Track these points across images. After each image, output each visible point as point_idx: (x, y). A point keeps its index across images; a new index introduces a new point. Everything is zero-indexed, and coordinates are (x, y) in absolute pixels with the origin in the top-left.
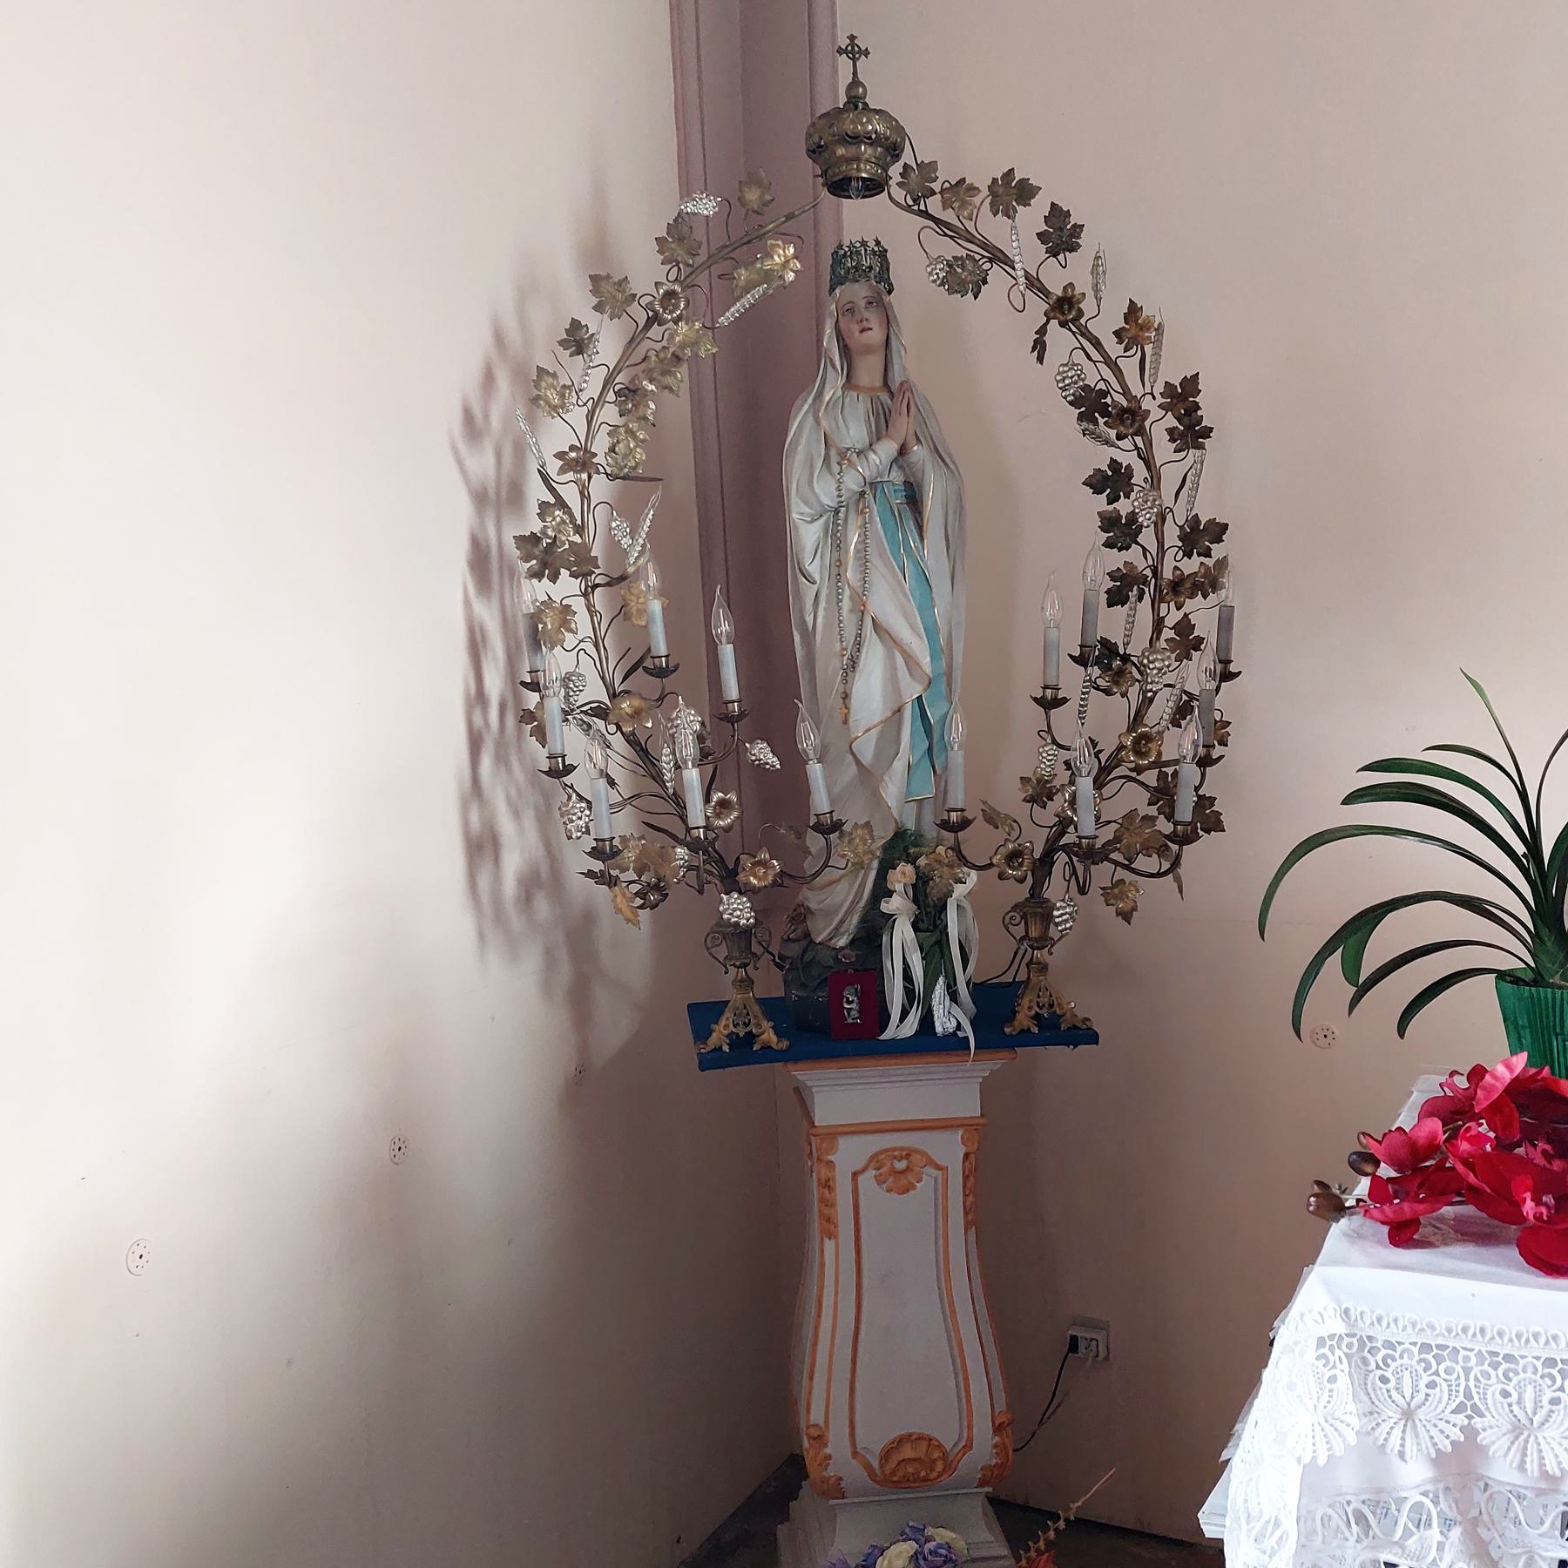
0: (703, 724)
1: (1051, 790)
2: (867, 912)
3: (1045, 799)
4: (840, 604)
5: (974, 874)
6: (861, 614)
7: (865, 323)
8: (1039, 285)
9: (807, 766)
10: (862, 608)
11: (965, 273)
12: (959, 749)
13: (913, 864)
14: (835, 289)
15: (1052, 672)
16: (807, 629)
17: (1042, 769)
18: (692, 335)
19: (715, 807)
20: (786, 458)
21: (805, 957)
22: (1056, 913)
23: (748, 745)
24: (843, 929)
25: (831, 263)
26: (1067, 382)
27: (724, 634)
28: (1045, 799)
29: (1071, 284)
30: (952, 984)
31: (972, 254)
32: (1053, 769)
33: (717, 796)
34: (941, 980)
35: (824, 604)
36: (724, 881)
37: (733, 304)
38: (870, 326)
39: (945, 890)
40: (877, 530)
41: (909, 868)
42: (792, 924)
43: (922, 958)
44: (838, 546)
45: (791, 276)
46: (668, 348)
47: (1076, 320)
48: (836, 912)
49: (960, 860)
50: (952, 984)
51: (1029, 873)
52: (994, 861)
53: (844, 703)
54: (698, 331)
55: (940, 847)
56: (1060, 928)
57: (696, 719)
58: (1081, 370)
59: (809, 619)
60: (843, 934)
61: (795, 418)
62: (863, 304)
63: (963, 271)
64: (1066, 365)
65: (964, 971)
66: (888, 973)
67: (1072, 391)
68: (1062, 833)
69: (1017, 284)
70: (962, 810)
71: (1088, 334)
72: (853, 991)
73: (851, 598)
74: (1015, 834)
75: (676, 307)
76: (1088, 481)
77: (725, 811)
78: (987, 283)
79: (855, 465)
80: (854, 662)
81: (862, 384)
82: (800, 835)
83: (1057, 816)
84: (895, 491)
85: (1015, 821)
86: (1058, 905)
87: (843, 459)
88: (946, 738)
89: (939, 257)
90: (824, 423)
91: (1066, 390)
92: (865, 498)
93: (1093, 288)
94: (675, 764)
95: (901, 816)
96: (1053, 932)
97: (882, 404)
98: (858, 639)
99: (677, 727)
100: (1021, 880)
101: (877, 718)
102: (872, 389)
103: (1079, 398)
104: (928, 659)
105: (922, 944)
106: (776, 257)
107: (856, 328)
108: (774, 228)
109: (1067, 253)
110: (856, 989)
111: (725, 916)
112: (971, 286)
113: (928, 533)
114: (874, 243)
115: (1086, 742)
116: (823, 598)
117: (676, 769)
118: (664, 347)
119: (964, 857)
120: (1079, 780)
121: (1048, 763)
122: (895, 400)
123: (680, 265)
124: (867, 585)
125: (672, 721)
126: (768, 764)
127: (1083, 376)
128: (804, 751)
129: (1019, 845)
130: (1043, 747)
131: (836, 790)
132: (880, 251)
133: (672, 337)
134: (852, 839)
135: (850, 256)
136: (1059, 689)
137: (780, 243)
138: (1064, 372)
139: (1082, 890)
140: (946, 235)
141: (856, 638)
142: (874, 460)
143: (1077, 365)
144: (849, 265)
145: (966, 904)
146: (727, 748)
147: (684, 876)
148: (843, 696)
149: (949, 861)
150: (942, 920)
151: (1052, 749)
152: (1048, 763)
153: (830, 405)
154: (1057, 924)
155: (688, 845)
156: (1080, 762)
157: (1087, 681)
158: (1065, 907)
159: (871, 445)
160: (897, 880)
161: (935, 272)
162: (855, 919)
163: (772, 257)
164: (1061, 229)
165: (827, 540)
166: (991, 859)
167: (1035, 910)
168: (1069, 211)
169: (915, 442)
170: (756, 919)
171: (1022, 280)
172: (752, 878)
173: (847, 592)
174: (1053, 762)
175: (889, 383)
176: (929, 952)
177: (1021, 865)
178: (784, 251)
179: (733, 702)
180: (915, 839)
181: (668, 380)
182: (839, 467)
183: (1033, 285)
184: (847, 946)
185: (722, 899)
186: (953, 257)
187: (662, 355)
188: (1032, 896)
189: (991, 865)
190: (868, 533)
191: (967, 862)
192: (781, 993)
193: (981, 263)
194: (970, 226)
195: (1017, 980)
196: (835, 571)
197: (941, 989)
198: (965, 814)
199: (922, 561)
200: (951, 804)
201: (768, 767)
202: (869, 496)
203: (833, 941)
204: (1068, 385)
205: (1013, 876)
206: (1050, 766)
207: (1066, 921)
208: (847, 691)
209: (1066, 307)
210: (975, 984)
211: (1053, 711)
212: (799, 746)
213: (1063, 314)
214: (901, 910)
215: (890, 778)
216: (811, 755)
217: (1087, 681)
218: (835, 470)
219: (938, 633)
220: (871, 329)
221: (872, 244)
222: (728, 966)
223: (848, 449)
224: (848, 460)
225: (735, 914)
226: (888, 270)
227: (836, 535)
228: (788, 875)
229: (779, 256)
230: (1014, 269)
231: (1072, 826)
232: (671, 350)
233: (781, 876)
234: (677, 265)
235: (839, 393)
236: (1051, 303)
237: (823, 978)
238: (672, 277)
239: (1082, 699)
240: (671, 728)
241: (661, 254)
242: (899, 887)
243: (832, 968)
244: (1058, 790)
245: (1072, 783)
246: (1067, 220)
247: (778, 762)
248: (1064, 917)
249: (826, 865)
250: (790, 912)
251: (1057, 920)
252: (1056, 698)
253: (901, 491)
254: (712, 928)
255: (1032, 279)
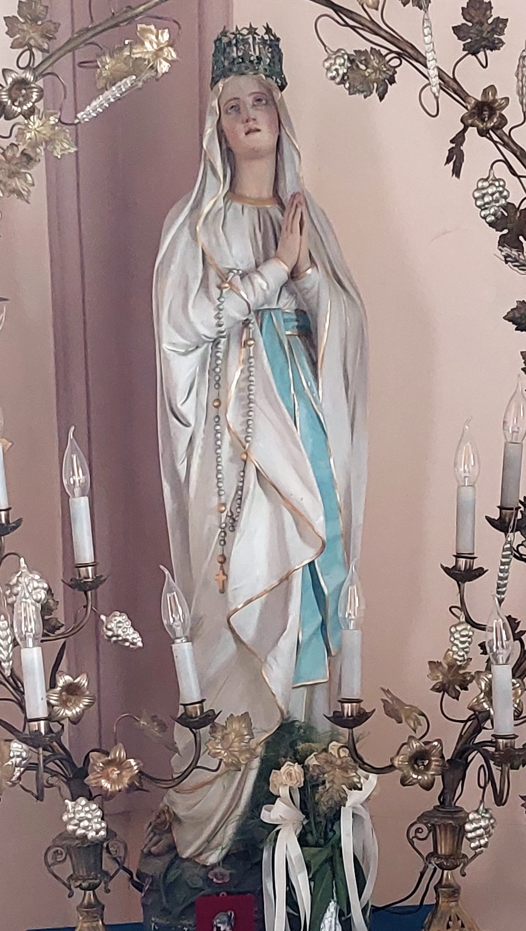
0: (49, 591)
1: (465, 678)
2: (246, 821)
3: (458, 688)
4: (219, 451)
5: (373, 777)
6: (243, 463)
7: (251, 123)
8: (455, 87)
9: (173, 646)
10: (245, 457)
11: (369, 70)
12: (357, 627)
13: (301, 762)
14: (218, 81)
15: (466, 539)
16: (179, 481)
17: (454, 652)
18: (46, 131)
19: (61, 692)
20: (157, 282)
21: (168, 877)
22: (468, 827)
23: (103, 617)
24: (215, 842)
25: (213, 52)
26: (487, 199)
27: (77, 484)
28: (458, 688)
29: (492, 86)
30: (345, 910)
31: (377, 48)
32: (467, 653)
33: (63, 680)
34: (332, 907)
35: (199, 451)
36: (72, 783)
37: (95, 98)
38: (259, 128)
39: (337, 798)
40: (263, 365)
41: (297, 768)
42: (155, 834)
43: (310, 880)
44: (217, 383)
45: (164, 67)
46: (17, 146)
47: (498, 129)
48: (209, 819)
49: (355, 761)
50: (345, 910)
51: (439, 779)
52: (396, 763)
53: (222, 568)
54: (54, 126)
55: (334, 743)
56: (473, 845)
57: (41, 585)
58: (503, 187)
59: (182, 468)
60: (216, 848)
61: (169, 228)
62: (250, 100)
63: (367, 68)
64: (486, 180)
65: (360, 897)
66: (269, 895)
67: (492, 211)
68: (478, 729)
69: (429, 84)
70: (359, 701)
71: (511, 144)
72: (225, 919)
73: (232, 444)
74: (421, 730)
75: (28, 98)
76: (509, 316)
77: (73, 698)
78: (394, 82)
79: (238, 290)
80: (234, 520)
81: (248, 195)
82: (163, 727)
83: (471, 708)
84: (285, 321)
85: (423, 715)
86: (471, 816)
87: (223, 281)
88: (340, 615)
89: (339, 50)
90: (202, 239)
91: (486, 209)
92: (250, 328)
93: (518, 93)
94: (14, 640)
95: (287, 705)
96: (466, 849)
97: (271, 218)
98: (240, 492)
99: (16, 595)
100: (428, 787)
101: (261, 588)
102: (260, 200)
103: (502, 218)
104: (322, 518)
105: (310, 862)
106: (147, 44)
107: (241, 129)
108: (145, 10)
109: (488, 52)
110: (229, 917)
111: (70, 828)
112: (375, 85)
113: (325, 364)
114: (265, 31)
115: (504, 624)
116: (198, 442)
117: (14, 646)
118: (12, 144)
119: (361, 759)
120: (495, 668)
121: (461, 646)
122: (286, 214)
123: (34, 50)
124: (250, 430)
125: (11, 587)
126: (126, 640)
127: (505, 193)
128: (171, 626)
129: (426, 743)
130: (455, 626)
131: (212, 672)
132: (271, 40)
133: (22, 133)
134: (227, 734)
135: (236, 45)
136: (474, 558)
137: (152, 27)
138: (483, 188)
139: (499, 800)
140: (347, 25)
141: (237, 492)
142: (260, 285)
143: (498, 180)
144: (235, 55)
145: (365, 814)
146: (78, 622)
147: (19, 778)
148: (221, 559)
149: (342, 762)
150: (334, 832)
151: (465, 629)
152: (461, 646)
153: (210, 217)
154: (471, 840)
155: (23, 741)
156: (497, 648)
157: (507, 549)
158: (479, 820)
159: (257, 266)
160: (282, 783)
161: (333, 68)
162: (230, 830)
163: (143, 44)
164: (481, 24)
165: (204, 375)
166: (392, 760)
167: (443, 821)
168: (490, 2)
169: (308, 264)
170: (107, 830)
171: (435, 81)
172: (103, 781)
173: (227, 437)
174: (467, 644)
175: (280, 194)
176: (317, 871)
177: (427, 768)
178: (157, 37)
179: (86, 566)
180: (305, 732)
181: (17, 183)
182: (219, 291)
183: (448, 87)
184: (219, 863)
185: (67, 806)
186: (355, 51)
187: (9, 154)
188: (442, 803)
189: (391, 767)
190: (252, 369)
191: (365, 763)
192: (139, 918)
193: (388, 58)
194: (376, 15)
195: (425, 903)
196: (213, 412)
197: (332, 917)
198: (362, 705)
199: (316, 403)
200: (346, 695)
201: (127, 644)
202: (254, 326)
203: (203, 857)
204: (488, 203)
205: (418, 781)
206: (463, 649)
207: (481, 837)
208: (226, 555)
209: (486, 113)
210: (375, 909)
211: (467, 583)
212: (165, 622)
213: (483, 121)
214: (285, 820)
215: (275, 658)
216: (179, 631)
217: (507, 549)
218: (214, 295)
219: (334, 487)
220: (259, 130)
221: (261, 31)
222: (72, 887)
223: (231, 270)
224: (230, 283)
225: (82, 824)
226: (280, 61)
227: (214, 370)
228: (148, 776)
229: (151, 43)
230: (426, 66)
231: (489, 721)
232: (21, 148)
233: (140, 778)
234: (30, 49)
235: (221, 204)
236: (469, 108)
237: (190, 901)
238: (23, 63)
239: (501, 571)
240: (10, 596)
241: (11, 37)
242: (284, 792)
243: (201, 890)
244: (473, 677)
245: (488, 669)
246: (488, 12)
247: (140, 639)
248: (479, 832)
249: (194, 766)
250: (153, 818)
251: (470, 835)
252: (471, 567)
253: (292, 320)
254: (54, 840)
255: (447, 79)
